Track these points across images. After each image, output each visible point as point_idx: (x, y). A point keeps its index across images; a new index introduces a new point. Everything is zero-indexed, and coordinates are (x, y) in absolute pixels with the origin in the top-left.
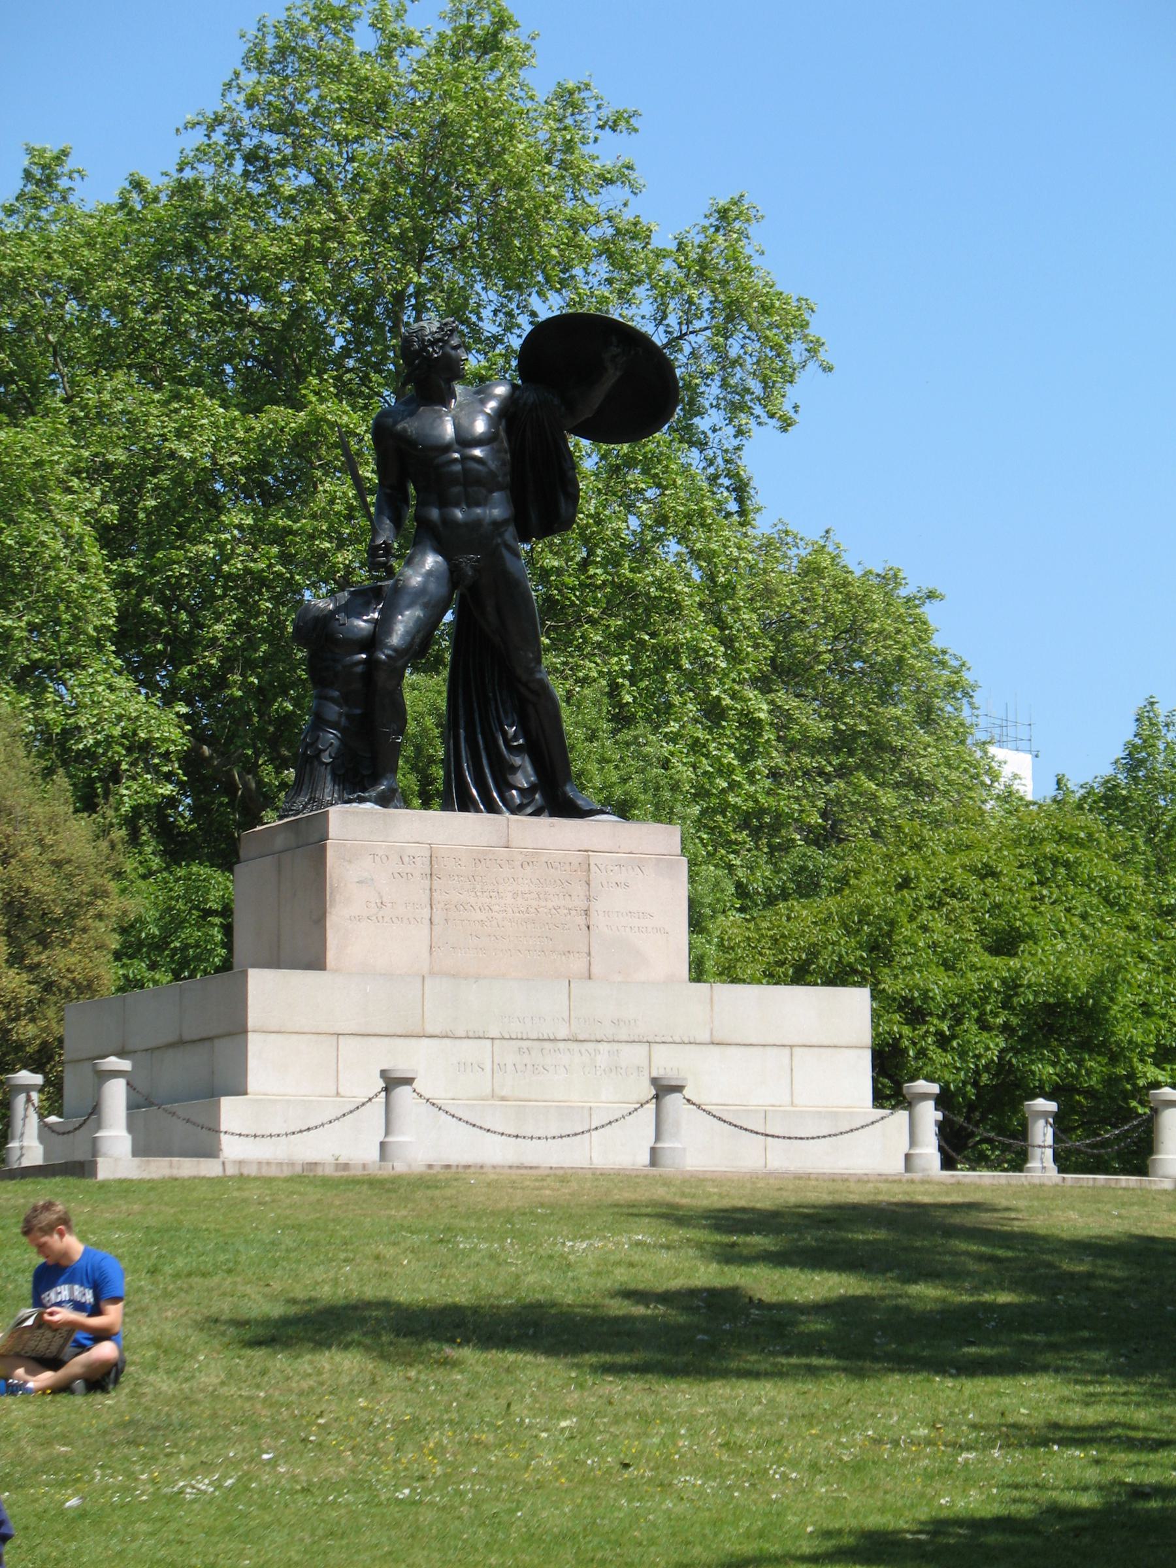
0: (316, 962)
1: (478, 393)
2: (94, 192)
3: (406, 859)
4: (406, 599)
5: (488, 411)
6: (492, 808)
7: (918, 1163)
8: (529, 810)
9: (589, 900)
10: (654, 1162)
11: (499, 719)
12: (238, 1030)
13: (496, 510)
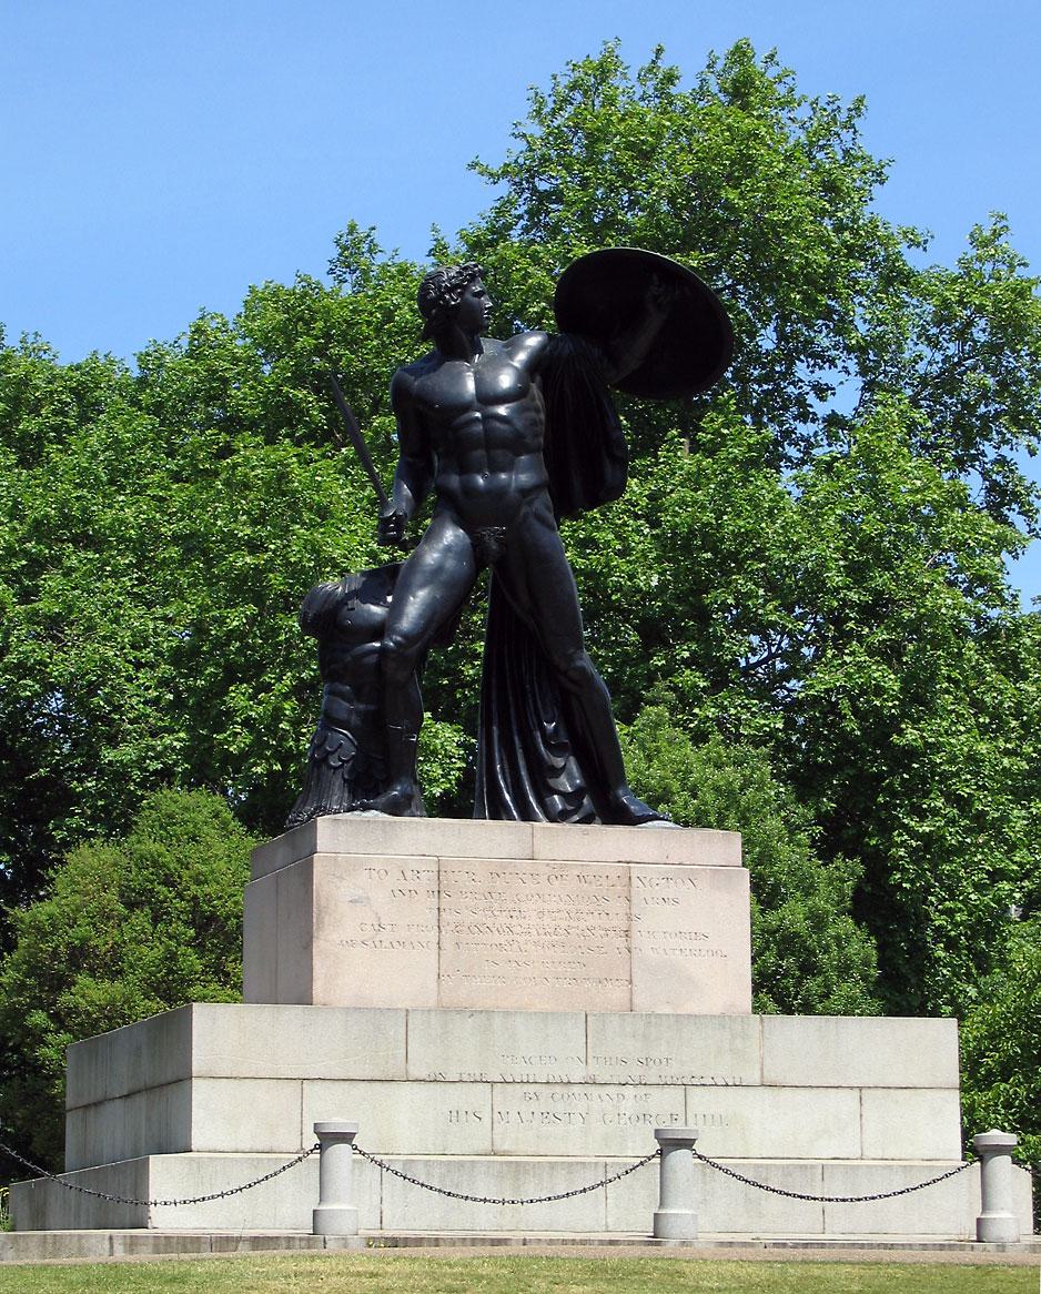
0: (302, 996)
1: (506, 346)
3: (408, 874)
4: (419, 578)
5: (516, 364)
6: (527, 815)
7: (993, 1232)
8: (576, 818)
9: (630, 919)
11: (538, 716)
12: (183, 1079)
13: (521, 476)
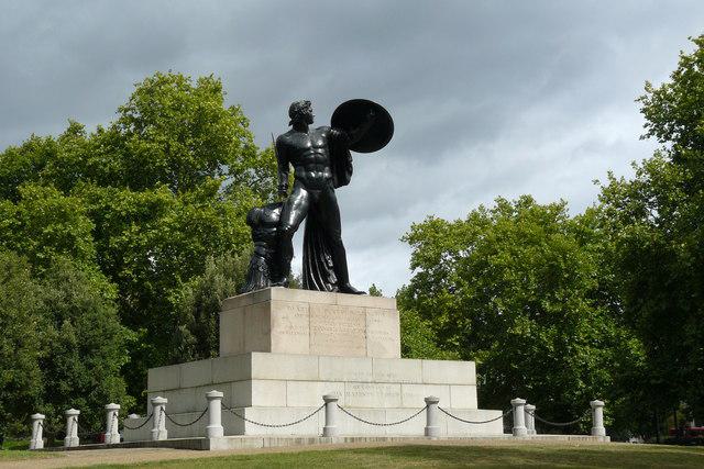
2: (90, 130)
6: (322, 289)
10: (325, 435)
